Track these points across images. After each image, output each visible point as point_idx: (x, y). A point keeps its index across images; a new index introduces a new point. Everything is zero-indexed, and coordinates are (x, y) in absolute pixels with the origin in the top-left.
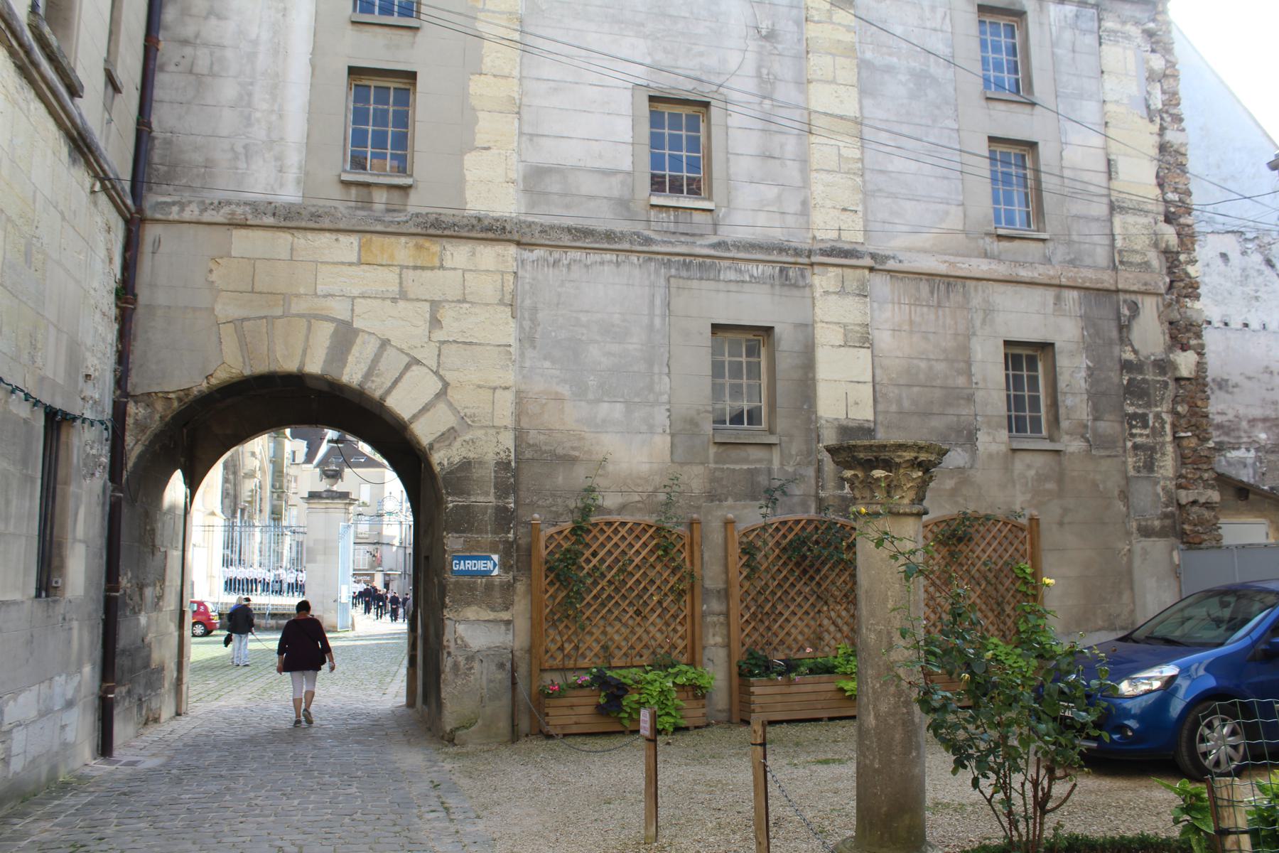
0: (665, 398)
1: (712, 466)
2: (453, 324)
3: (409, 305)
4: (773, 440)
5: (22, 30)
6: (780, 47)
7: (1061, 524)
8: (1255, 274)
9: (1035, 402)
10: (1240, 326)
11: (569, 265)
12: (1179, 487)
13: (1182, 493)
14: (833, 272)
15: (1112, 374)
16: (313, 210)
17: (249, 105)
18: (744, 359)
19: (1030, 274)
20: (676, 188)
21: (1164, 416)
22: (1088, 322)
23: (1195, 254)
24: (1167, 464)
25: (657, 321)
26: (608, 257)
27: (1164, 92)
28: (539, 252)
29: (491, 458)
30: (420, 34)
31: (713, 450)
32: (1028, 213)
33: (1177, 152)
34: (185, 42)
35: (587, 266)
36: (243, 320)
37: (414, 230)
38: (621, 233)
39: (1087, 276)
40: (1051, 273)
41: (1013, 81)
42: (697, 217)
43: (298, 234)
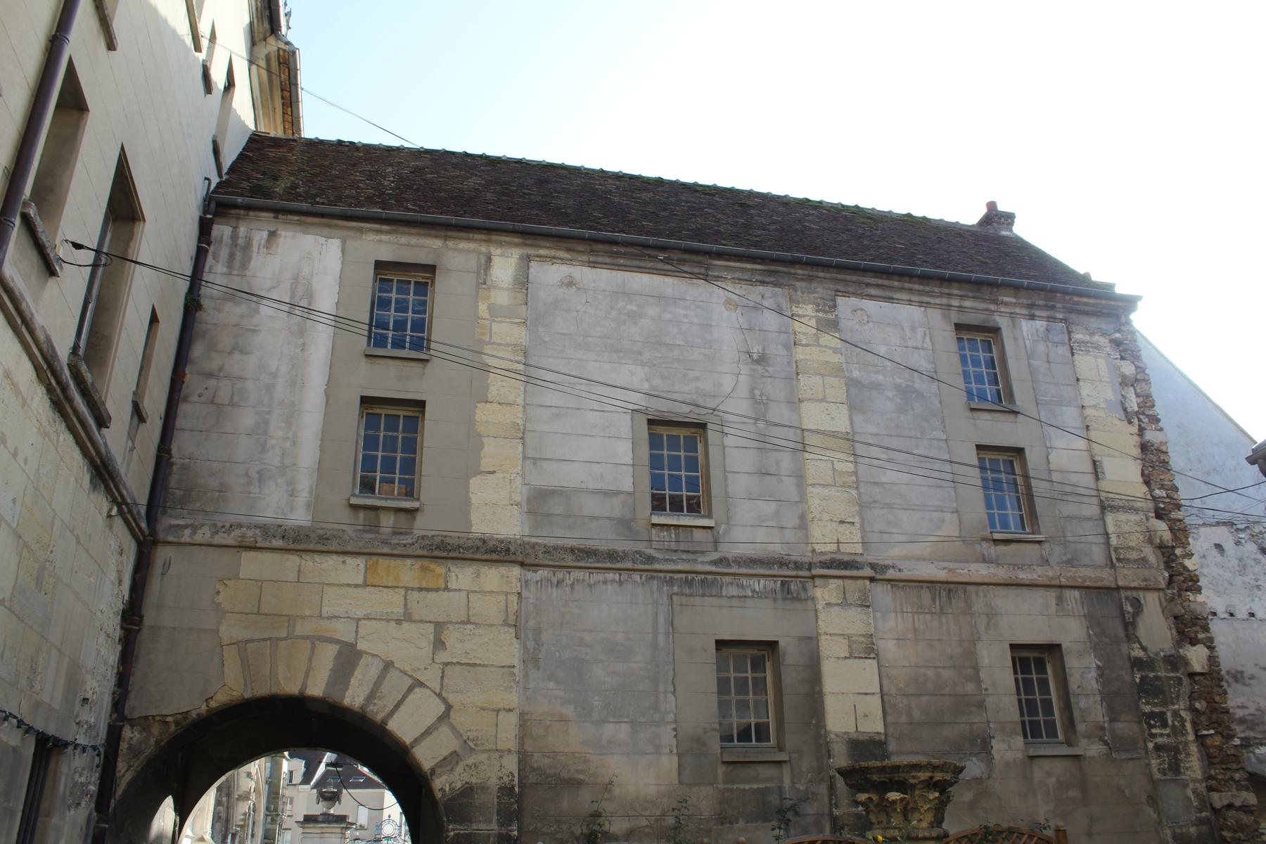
0: (671, 717)
1: (721, 786)
2: (456, 647)
3: (414, 627)
4: (783, 757)
5: (62, 370)
6: (770, 369)
7: (1090, 834)
8: (1253, 563)
9: (1047, 704)
10: (1246, 616)
11: (572, 585)
12: (1210, 789)
13: (1215, 796)
14: (834, 584)
15: (1123, 673)
16: (322, 533)
17: (265, 432)
18: (749, 675)
19: (1030, 576)
20: (676, 506)
21: (1183, 714)
22: (1092, 620)
23: (1190, 547)
24: (1194, 765)
25: (661, 640)
26: (610, 576)
27: (1137, 395)
28: (543, 573)
29: (494, 782)
30: (429, 365)
31: (721, 770)
32: (1021, 516)
33: (1158, 450)
34: (210, 375)
35: (590, 586)
36: (247, 642)
37: (419, 552)
38: (624, 552)
39: (1086, 574)
40: (1051, 574)
41: (994, 392)
42: (698, 534)
43: (306, 556)
